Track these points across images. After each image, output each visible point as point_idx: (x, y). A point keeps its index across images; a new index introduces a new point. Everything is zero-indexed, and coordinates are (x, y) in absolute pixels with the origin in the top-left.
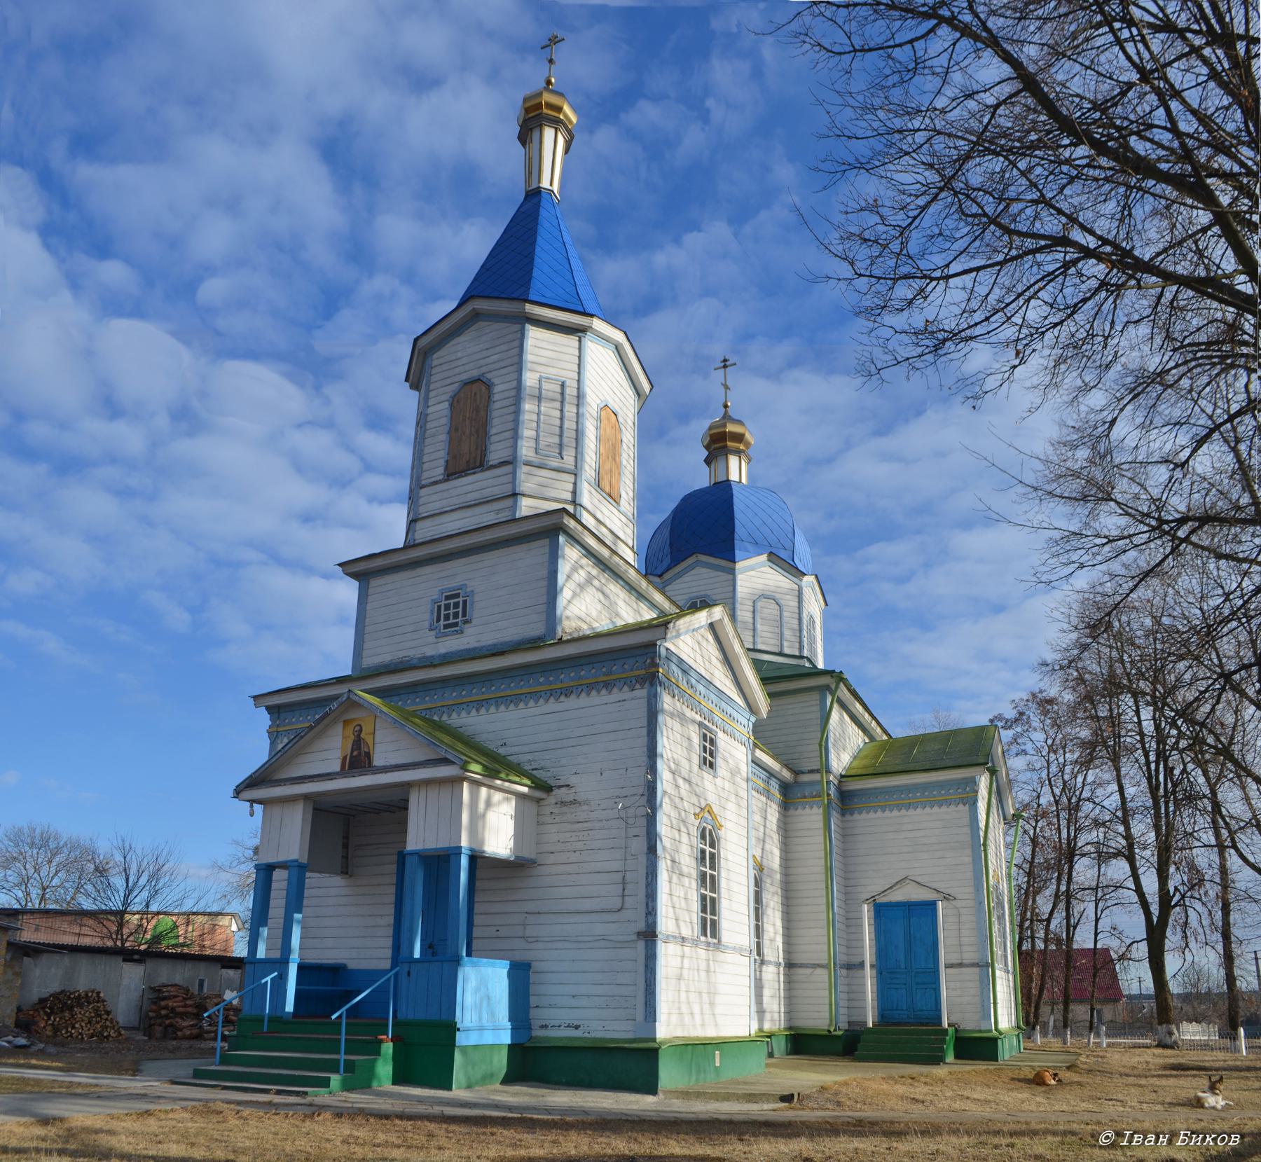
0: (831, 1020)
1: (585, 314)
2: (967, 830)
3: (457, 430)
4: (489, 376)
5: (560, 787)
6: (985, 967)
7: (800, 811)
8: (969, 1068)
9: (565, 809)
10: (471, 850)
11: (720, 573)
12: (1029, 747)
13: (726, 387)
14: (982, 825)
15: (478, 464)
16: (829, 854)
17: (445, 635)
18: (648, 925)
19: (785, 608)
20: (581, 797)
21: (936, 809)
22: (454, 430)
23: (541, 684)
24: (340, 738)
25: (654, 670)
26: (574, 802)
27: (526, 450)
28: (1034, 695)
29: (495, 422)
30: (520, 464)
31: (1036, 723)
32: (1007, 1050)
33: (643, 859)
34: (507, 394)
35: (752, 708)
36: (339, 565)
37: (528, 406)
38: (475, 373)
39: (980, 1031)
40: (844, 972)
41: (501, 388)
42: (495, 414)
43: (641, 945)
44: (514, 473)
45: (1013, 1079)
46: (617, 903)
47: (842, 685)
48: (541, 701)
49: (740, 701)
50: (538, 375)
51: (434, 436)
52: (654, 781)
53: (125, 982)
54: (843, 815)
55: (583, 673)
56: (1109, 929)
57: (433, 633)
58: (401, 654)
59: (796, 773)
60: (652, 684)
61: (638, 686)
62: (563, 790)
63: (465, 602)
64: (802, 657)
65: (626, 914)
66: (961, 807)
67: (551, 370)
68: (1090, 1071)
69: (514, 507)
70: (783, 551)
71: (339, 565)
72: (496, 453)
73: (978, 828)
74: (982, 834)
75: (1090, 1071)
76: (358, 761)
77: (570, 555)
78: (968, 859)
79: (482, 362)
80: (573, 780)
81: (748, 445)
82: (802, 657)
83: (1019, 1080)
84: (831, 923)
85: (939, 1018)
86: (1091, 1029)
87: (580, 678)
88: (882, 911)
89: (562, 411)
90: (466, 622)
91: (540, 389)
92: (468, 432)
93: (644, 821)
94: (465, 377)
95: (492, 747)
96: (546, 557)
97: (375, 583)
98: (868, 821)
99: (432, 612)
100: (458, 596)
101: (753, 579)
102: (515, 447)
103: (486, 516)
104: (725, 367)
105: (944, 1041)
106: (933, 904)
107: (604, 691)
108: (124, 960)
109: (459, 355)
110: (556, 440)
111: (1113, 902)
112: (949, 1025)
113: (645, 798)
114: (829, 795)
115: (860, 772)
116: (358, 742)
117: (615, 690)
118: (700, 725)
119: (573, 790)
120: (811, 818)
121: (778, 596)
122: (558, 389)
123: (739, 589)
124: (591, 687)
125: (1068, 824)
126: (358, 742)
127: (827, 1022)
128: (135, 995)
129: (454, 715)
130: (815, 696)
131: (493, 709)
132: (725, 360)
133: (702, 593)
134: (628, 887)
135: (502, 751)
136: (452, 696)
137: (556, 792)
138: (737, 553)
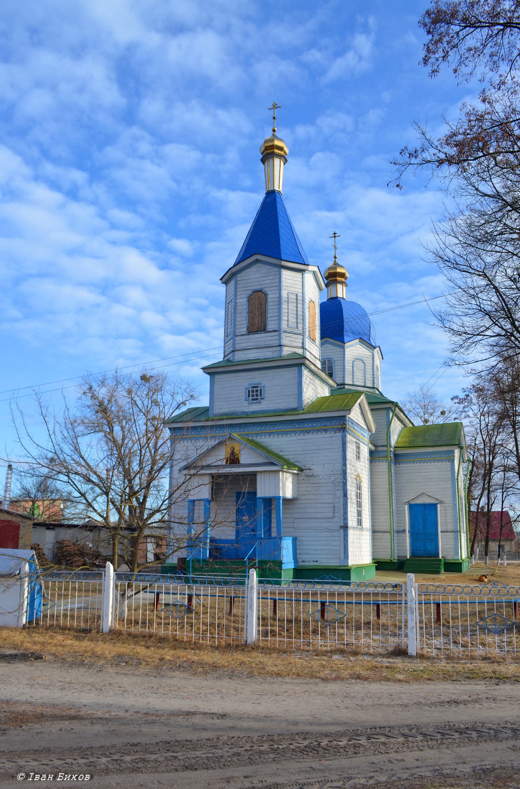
0: (392, 556)
1: (305, 264)
2: (450, 473)
3: (252, 312)
4: (265, 290)
5: (306, 469)
6: (456, 532)
7: (377, 464)
8: (456, 575)
9: (309, 478)
10: (283, 497)
11: (337, 348)
12: (471, 413)
13: (336, 248)
14: (456, 470)
15: (263, 329)
16: (390, 484)
17: (252, 403)
18: (344, 524)
19: (366, 364)
20: (316, 474)
21: (436, 463)
22: (250, 312)
23: (297, 428)
24: (224, 451)
25: (344, 426)
26: (313, 476)
27: (284, 325)
28: (474, 386)
29: (269, 311)
30: (282, 332)
31: (475, 401)
32: (465, 567)
33: (342, 499)
34: (274, 300)
35: (369, 430)
36: (202, 369)
37: (284, 306)
38: (258, 287)
39: (455, 560)
40: (396, 534)
41: (271, 296)
42: (269, 308)
43: (342, 531)
44: (280, 335)
45: (470, 579)
46: (331, 515)
47: (397, 408)
48: (297, 434)
49: (365, 427)
50: (287, 292)
51: (241, 313)
52: (346, 469)
53: (47, 539)
54: (395, 464)
55: (314, 425)
56: (508, 506)
57: (247, 402)
58: (233, 409)
59: (376, 446)
60: (344, 431)
61: (338, 432)
62: (308, 471)
63: (261, 390)
64: (374, 388)
65: (335, 519)
66: (447, 463)
67: (292, 289)
68: (500, 576)
69: (281, 351)
70: (365, 336)
71: (202, 369)
72: (271, 326)
73: (455, 472)
74: (456, 474)
75: (500, 576)
76: (233, 460)
77: (305, 373)
78: (450, 486)
79: (261, 282)
80: (312, 467)
81: (346, 278)
82: (374, 388)
83: (474, 580)
84: (391, 513)
85: (438, 554)
86: (499, 557)
87: (314, 427)
88: (412, 507)
89: (297, 307)
90: (262, 399)
91: (288, 298)
92: (257, 314)
93: (342, 484)
94: (254, 288)
95: (277, 452)
96: (297, 375)
97: (217, 377)
98: (406, 467)
99: (246, 393)
100: (257, 387)
101: (353, 351)
102: (280, 324)
103: (268, 354)
104: (335, 237)
105: (440, 564)
106: (435, 506)
107: (324, 433)
108: (47, 529)
109: (251, 277)
110: (295, 321)
111: (511, 493)
112: (442, 557)
113: (342, 476)
114: (391, 457)
115: (403, 445)
116: (233, 453)
117: (328, 432)
118: (356, 442)
119: (312, 471)
120: (383, 466)
121: (363, 359)
122: (295, 297)
123: (346, 356)
124: (318, 431)
125: (490, 452)
126: (233, 453)
127: (390, 556)
128: (51, 546)
129: (259, 437)
130: (385, 412)
131: (276, 436)
132: (335, 234)
133: (329, 357)
134: (336, 509)
135: (281, 454)
136: (257, 429)
137: (305, 471)
138: (346, 339)
